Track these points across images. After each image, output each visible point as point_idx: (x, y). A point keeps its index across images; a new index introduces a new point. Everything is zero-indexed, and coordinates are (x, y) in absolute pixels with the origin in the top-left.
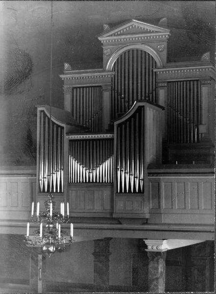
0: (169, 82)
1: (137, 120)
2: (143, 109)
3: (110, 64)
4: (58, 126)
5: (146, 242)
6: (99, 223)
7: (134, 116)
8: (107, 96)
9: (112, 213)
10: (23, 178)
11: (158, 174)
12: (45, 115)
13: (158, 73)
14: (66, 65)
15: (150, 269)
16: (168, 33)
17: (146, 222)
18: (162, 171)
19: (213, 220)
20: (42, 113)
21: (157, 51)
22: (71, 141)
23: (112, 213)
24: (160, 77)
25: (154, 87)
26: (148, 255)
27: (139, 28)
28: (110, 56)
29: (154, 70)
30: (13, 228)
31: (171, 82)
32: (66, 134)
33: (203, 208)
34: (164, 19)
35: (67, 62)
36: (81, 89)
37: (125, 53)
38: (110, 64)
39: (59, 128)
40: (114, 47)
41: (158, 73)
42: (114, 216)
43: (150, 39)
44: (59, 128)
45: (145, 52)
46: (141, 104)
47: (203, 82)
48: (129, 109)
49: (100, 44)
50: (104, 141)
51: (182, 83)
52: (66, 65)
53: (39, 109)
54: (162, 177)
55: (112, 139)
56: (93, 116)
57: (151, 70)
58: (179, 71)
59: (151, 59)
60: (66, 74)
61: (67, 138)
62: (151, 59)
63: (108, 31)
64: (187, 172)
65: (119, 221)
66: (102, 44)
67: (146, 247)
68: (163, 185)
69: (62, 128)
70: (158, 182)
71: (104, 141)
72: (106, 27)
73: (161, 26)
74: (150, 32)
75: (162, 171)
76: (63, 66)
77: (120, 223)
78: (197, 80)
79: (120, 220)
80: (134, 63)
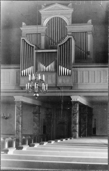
0: (72, 32)
1: (64, 47)
2: (70, 39)
3: (45, 22)
4: (31, 46)
5: (72, 97)
6: (53, 89)
7: (66, 42)
8: (43, 38)
9: (56, 85)
10: (13, 70)
11: (77, 67)
12: (25, 41)
13: (68, 28)
14: (24, 24)
15: (17, 101)
16: (73, 10)
17: (71, 88)
18: (78, 66)
19: (106, 87)
20: (23, 40)
21: (68, 18)
22: (37, 53)
23: (56, 85)
24: (68, 30)
25: (65, 35)
26: (72, 103)
27: (59, 7)
28: (45, 19)
29: (66, 27)
30: (7, 93)
31: (73, 32)
32: (35, 49)
33: (96, 82)
34: (71, 4)
35: (24, 22)
36: (30, 35)
37: (52, 19)
38: (45, 22)
39: (31, 47)
40: (48, 14)
41: (68, 28)
42: (58, 86)
43: (64, 12)
44: (31, 47)
45: (61, 19)
46: (70, 37)
47: (88, 33)
48: (65, 39)
49: (40, 15)
50: (48, 54)
51: (78, 33)
52: (24, 24)
53: (22, 38)
54: (78, 69)
55: (56, 52)
56: (62, 38)
57: (64, 27)
58: (79, 28)
59: (64, 22)
60: (23, 27)
61: (35, 51)
62: (64, 22)
63: (44, 8)
64: (103, 66)
65: (59, 88)
66: (41, 14)
67: (71, 99)
68: (79, 73)
69: (33, 47)
70: (77, 71)
71: (48, 54)
72: (43, 6)
73: (69, 7)
74: (64, 10)
75: (88, 66)
76: (22, 24)
77: (60, 89)
78: (85, 32)
79: (23, 88)
80: (57, 23)
